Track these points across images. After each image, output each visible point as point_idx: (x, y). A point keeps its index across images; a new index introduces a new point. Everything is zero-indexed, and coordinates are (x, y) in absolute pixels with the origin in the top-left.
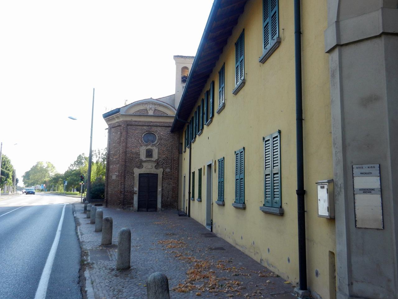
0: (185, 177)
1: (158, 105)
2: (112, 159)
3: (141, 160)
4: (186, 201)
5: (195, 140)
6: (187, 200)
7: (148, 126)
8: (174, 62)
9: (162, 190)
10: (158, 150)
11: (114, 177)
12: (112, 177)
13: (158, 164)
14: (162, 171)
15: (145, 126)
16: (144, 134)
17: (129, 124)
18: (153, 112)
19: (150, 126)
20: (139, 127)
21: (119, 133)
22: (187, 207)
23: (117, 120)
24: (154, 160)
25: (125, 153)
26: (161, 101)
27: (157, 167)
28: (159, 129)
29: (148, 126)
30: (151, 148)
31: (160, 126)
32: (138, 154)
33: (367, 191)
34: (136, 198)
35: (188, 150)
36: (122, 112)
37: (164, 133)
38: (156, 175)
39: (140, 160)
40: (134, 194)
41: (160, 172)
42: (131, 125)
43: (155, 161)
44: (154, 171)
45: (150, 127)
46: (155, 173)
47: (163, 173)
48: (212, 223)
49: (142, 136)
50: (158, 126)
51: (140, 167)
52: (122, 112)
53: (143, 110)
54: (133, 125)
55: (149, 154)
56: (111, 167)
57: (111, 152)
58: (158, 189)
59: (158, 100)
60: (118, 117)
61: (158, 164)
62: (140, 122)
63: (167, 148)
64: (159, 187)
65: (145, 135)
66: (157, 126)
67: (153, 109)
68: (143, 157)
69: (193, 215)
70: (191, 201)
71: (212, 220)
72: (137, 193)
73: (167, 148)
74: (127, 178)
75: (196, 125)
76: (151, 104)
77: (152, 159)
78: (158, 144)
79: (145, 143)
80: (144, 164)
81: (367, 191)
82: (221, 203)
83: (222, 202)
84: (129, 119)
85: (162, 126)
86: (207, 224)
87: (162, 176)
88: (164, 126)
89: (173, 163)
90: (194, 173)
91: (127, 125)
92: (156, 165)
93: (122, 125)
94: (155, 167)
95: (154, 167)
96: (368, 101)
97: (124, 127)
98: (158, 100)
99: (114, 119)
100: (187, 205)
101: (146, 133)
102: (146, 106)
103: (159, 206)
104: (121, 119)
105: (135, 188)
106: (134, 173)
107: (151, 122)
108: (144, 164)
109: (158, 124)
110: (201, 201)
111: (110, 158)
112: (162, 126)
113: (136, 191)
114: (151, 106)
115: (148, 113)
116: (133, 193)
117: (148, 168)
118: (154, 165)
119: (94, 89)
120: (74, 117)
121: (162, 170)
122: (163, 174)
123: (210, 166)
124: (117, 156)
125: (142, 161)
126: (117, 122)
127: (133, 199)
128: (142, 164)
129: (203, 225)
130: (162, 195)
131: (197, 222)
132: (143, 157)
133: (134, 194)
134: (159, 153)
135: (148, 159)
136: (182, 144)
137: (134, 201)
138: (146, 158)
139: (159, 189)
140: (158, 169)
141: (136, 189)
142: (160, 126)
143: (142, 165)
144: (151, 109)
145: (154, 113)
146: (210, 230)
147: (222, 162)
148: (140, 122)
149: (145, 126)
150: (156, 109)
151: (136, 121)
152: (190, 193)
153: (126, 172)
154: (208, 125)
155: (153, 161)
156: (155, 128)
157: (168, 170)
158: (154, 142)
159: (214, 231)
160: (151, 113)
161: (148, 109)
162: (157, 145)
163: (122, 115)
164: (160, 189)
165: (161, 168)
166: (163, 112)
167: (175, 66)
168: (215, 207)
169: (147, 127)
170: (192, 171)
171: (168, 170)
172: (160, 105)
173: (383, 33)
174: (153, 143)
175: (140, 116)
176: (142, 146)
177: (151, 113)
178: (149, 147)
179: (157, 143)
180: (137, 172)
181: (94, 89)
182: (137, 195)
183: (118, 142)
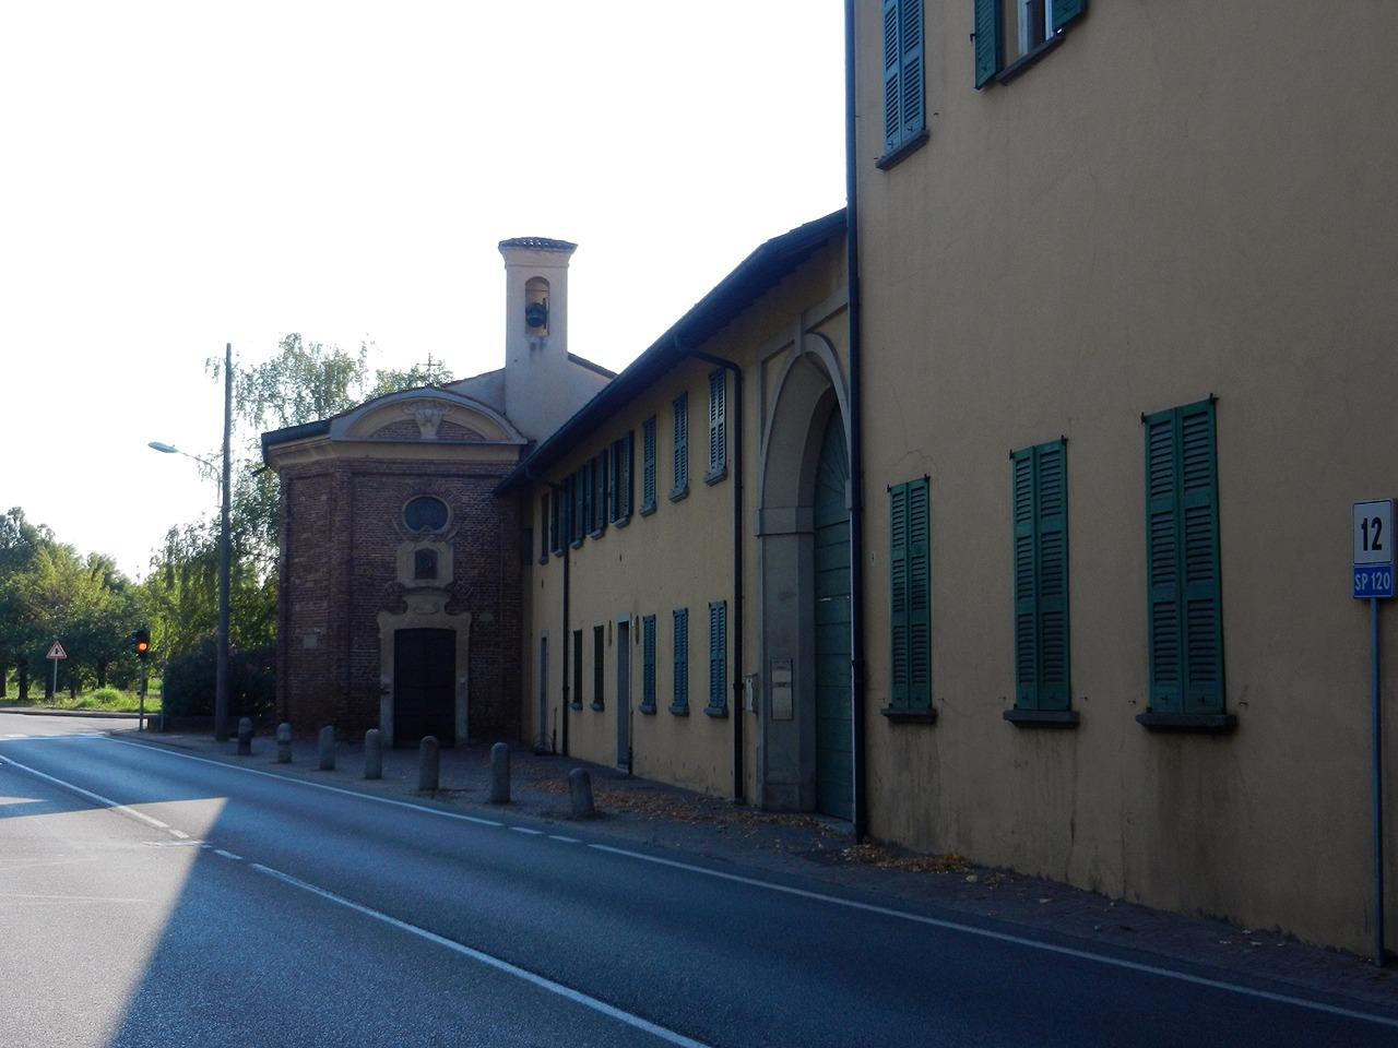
0: (544, 640)
1: (450, 406)
2: (298, 582)
3: (401, 586)
4: (550, 713)
5: (581, 545)
6: (556, 710)
7: (419, 475)
8: (499, 261)
9: (470, 680)
10: (455, 552)
11: (310, 642)
12: (301, 641)
13: (455, 598)
14: (469, 621)
15: (410, 475)
16: (406, 503)
17: (358, 472)
18: (435, 429)
19: (426, 474)
20: (391, 480)
21: (324, 497)
22: (555, 732)
23: (315, 457)
24: (443, 585)
25: (350, 563)
26: (460, 395)
27: (450, 609)
28: (459, 484)
29: (419, 475)
30: (431, 548)
31: (459, 476)
32: (390, 568)
33: (782, 685)
34: (386, 708)
35: (556, 563)
36: (336, 433)
37: (465, 498)
38: (450, 635)
39: (396, 588)
40: (382, 697)
41: (461, 622)
42: (364, 474)
43: (445, 590)
44: (440, 620)
45: (426, 478)
46: (447, 627)
47: (471, 626)
48: (631, 754)
49: (400, 508)
50: (454, 475)
51: (398, 607)
52: (336, 433)
53: (402, 423)
54: (372, 474)
55: (426, 565)
56: (297, 607)
57: (296, 560)
58: (457, 678)
59: (452, 392)
60: (319, 448)
61: (455, 598)
62: (394, 463)
63: (483, 545)
64: (458, 673)
65: (413, 501)
66: (449, 476)
67: (437, 420)
68: (406, 575)
69: (575, 750)
70: (572, 712)
71: (631, 748)
72: (388, 693)
73: (483, 545)
74: (356, 646)
75: (585, 508)
76: (428, 405)
77: (437, 583)
78: (454, 533)
79: (412, 531)
80: (410, 600)
81: (782, 685)
82: (649, 708)
83: (651, 709)
84: (357, 454)
85: (463, 476)
86: (620, 762)
87: (470, 638)
88: (470, 476)
89: (501, 596)
90: (578, 635)
91: (353, 473)
92: (447, 600)
93: (338, 475)
94: (446, 607)
95: (442, 609)
96: (785, 596)
97: (343, 483)
98: (452, 392)
99: (303, 451)
100: (555, 723)
101: (412, 499)
102: (413, 410)
103: (462, 730)
104: (332, 455)
105: (382, 677)
106: (378, 629)
107: (431, 462)
108: (410, 600)
109: (454, 470)
110: (602, 709)
111: (292, 579)
112: (463, 476)
113: (386, 686)
114: (428, 412)
115: (419, 432)
116: (376, 692)
117: (424, 612)
118: (443, 600)
119: (229, 346)
120: (169, 444)
121: (466, 617)
122: (472, 631)
123: (624, 626)
124: (319, 574)
125: (403, 590)
126: (317, 462)
127: (377, 711)
128: (405, 599)
129: (608, 767)
130: (470, 695)
131: (598, 766)
132: (406, 575)
133: (382, 697)
134: (457, 564)
135: (422, 583)
136: (530, 531)
137: (382, 717)
138: (417, 581)
139: (461, 679)
140: (455, 614)
141: (387, 679)
142: (459, 476)
143: (404, 602)
144: (430, 421)
145: (438, 433)
146: (627, 771)
147: (650, 622)
148: (394, 463)
149: (410, 475)
150: (446, 419)
151: (381, 462)
152: (566, 689)
153: (353, 624)
154: (620, 527)
155: (438, 589)
156: (444, 480)
157: (487, 617)
158: (440, 526)
159: (635, 772)
160: (429, 433)
161: (420, 418)
162: (450, 536)
163: (335, 441)
164: (463, 676)
165: (465, 610)
166: (469, 430)
167: (504, 273)
168: (638, 719)
169: (417, 481)
170: (573, 628)
171: (487, 617)
172: (458, 407)
173: (796, 533)
174: (438, 532)
175: (394, 444)
176: (400, 541)
177: (429, 433)
178: (425, 544)
179: (449, 531)
180: (388, 623)
181: (229, 346)
182: (391, 697)
183: (323, 529)
